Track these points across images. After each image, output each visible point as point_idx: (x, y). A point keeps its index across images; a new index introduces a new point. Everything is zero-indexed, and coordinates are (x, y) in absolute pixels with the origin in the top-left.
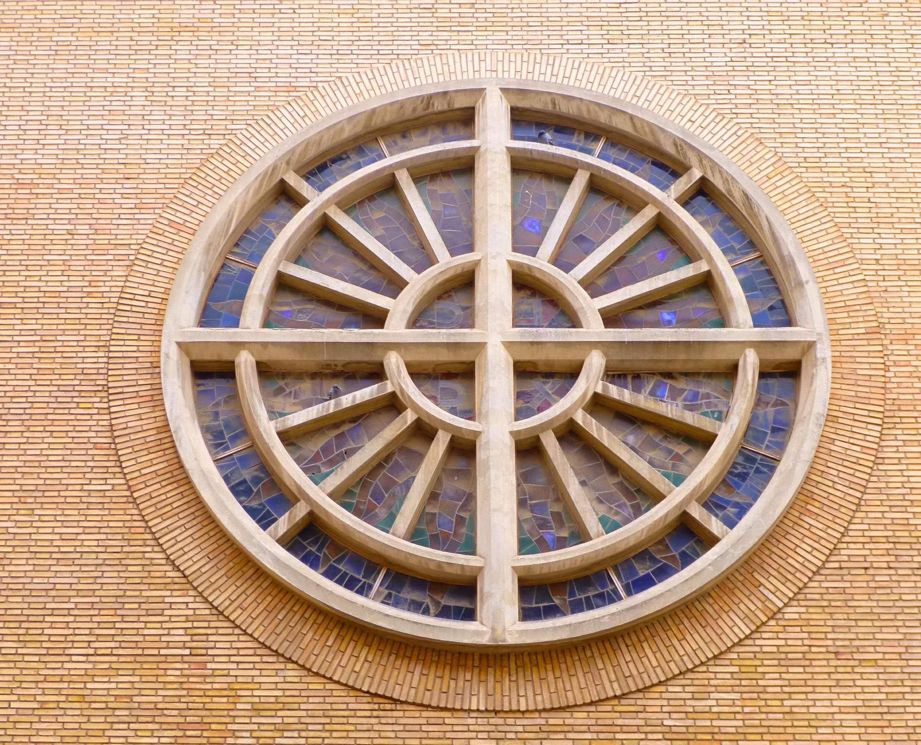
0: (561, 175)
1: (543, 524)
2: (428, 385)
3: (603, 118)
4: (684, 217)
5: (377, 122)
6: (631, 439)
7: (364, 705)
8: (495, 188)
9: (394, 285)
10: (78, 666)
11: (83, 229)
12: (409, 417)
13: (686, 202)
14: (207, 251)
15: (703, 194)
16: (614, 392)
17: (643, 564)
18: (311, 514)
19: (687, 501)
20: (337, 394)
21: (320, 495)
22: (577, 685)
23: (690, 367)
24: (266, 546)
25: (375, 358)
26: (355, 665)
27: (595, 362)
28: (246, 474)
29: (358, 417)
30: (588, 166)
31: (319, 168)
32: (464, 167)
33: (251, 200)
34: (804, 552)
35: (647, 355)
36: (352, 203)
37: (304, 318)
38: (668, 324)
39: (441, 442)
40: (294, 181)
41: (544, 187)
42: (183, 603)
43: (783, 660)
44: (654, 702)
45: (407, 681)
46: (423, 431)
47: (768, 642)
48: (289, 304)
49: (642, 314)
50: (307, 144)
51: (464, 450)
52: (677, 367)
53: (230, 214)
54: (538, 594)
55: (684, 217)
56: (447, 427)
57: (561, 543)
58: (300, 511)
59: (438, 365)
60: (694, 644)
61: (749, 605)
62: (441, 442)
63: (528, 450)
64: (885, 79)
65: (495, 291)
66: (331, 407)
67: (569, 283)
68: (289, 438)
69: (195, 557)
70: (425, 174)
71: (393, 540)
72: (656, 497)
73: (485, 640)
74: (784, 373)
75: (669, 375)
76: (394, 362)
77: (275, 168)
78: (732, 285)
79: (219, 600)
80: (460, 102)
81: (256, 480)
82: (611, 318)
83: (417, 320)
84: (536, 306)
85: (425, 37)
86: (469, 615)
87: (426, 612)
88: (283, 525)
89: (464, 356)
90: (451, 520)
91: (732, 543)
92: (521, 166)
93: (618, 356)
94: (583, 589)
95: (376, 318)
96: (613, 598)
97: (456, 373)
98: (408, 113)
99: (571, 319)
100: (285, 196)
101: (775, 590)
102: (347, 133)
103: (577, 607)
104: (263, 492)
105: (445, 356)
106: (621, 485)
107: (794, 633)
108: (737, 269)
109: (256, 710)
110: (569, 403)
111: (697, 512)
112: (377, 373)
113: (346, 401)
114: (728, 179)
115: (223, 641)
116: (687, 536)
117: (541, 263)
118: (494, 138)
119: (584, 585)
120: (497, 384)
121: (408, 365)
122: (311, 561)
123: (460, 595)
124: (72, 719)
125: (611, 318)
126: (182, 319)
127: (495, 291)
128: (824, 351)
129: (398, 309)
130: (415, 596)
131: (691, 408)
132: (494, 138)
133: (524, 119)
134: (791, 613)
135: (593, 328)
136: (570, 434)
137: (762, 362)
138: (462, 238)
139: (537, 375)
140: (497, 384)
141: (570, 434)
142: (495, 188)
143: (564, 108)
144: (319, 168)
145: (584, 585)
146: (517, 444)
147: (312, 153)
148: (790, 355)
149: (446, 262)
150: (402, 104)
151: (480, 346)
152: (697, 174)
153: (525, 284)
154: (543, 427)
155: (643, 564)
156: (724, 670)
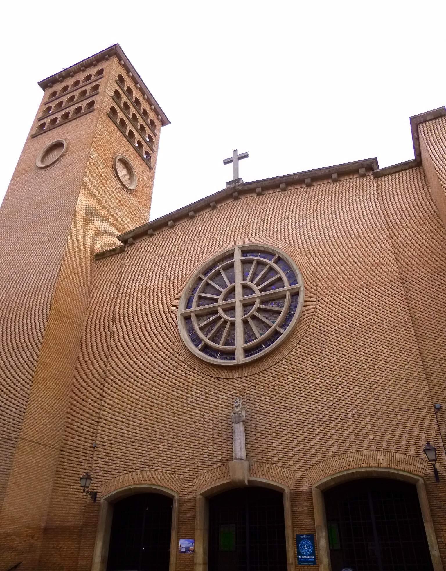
0: (250, 262)
1: (249, 337)
2: (227, 313)
3: (258, 248)
4: (275, 266)
5: (216, 260)
6: (266, 315)
7: (216, 380)
8: (238, 268)
9: (219, 293)
10: (166, 380)
11: (166, 294)
12: (223, 320)
13: (276, 262)
14: (185, 294)
15: (279, 260)
16: (261, 306)
17: (267, 341)
18: (205, 343)
19: (276, 326)
20: (209, 318)
21: (206, 340)
22: (256, 369)
23: (277, 298)
24: (196, 351)
25: (216, 309)
26: (214, 373)
27: (258, 301)
28: (195, 337)
29: (215, 322)
30: (220, 268)
31: (206, 273)
32: (232, 265)
33: (193, 282)
34: (300, 333)
35: (267, 297)
36: (212, 279)
37: (204, 303)
38: (274, 289)
39: (229, 323)
40: (201, 276)
41: (230, 270)
42: (184, 365)
43: (297, 357)
44: (271, 370)
45: (224, 374)
46: (226, 322)
47: (293, 354)
48: (202, 301)
49: (268, 288)
50: (203, 268)
51: (233, 324)
52: (275, 298)
53: (189, 286)
54: (248, 352)
55: (275, 266)
56: (229, 321)
57: (253, 340)
58: (203, 343)
59: (228, 308)
60: (278, 357)
61: (290, 346)
62: (229, 323)
63: (245, 322)
64: (316, 225)
65: (239, 290)
66: (208, 321)
67: (253, 285)
68: (201, 329)
69: (186, 356)
70: (225, 269)
71: (220, 346)
72: (270, 327)
73: (236, 364)
74: (295, 295)
75: (274, 300)
76: (220, 309)
77: (197, 275)
78: (285, 278)
79: (190, 363)
80: (231, 252)
81: (196, 338)
82: (261, 291)
83: (225, 299)
84: (248, 291)
85: (226, 240)
86: (234, 359)
87: (228, 360)
88: (200, 347)
89: (232, 305)
90: (231, 341)
91: (285, 333)
92: (244, 262)
93: (262, 298)
94: (257, 349)
95: (216, 300)
96: (216, 358)
97: (230, 309)
98: (222, 257)
99: (253, 292)
100: (201, 279)
101: (294, 342)
102: (210, 264)
103: (256, 353)
104: (196, 340)
105: (229, 306)
106: (264, 326)
107: (299, 351)
108: (286, 274)
109: (197, 384)
110: (253, 311)
111: (278, 329)
112: (217, 312)
113: (211, 319)
114: (283, 256)
115: (190, 371)
116: (277, 334)
117: (248, 282)
118: (238, 257)
119: (257, 348)
120: (239, 310)
121: (223, 309)
122: (206, 353)
123: (232, 355)
124: (165, 391)
125: (261, 291)
126: (182, 309)
127: (239, 290)
128: (302, 288)
129: (220, 298)
130: (225, 356)
131: (278, 306)
132: (238, 257)
133: (244, 252)
134: (298, 346)
135: (258, 294)
136: (254, 317)
137: (291, 294)
138: (232, 281)
139: (247, 306)
140: (239, 310)
141: (254, 317)
142: (238, 268)
143: (251, 248)
144: (206, 273)
145: (257, 348)
146: (243, 321)
147: (204, 270)
148: (296, 290)
149: (229, 285)
150: (220, 255)
151: (235, 302)
152: (277, 256)
153: (245, 287)
154: (248, 317)
155: (267, 341)
156: (284, 361)
